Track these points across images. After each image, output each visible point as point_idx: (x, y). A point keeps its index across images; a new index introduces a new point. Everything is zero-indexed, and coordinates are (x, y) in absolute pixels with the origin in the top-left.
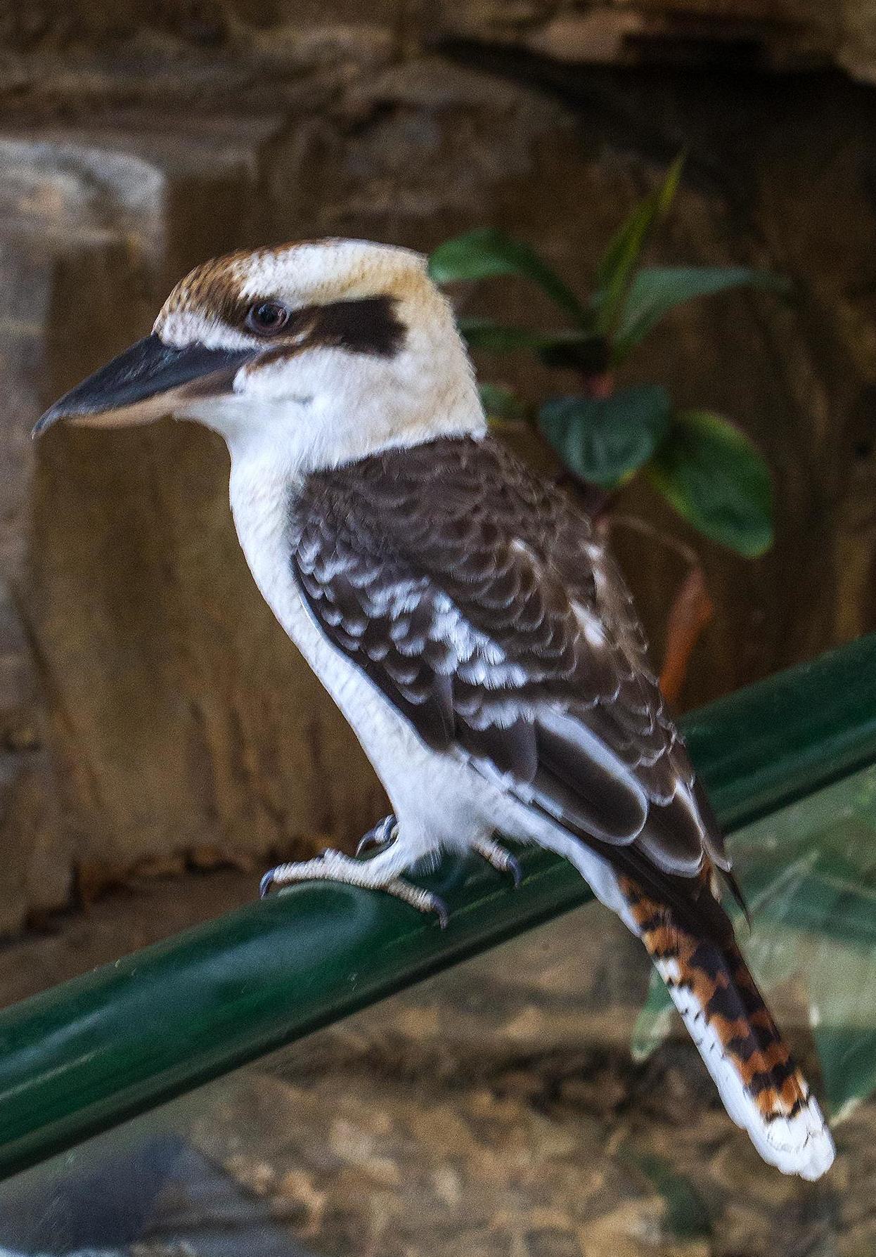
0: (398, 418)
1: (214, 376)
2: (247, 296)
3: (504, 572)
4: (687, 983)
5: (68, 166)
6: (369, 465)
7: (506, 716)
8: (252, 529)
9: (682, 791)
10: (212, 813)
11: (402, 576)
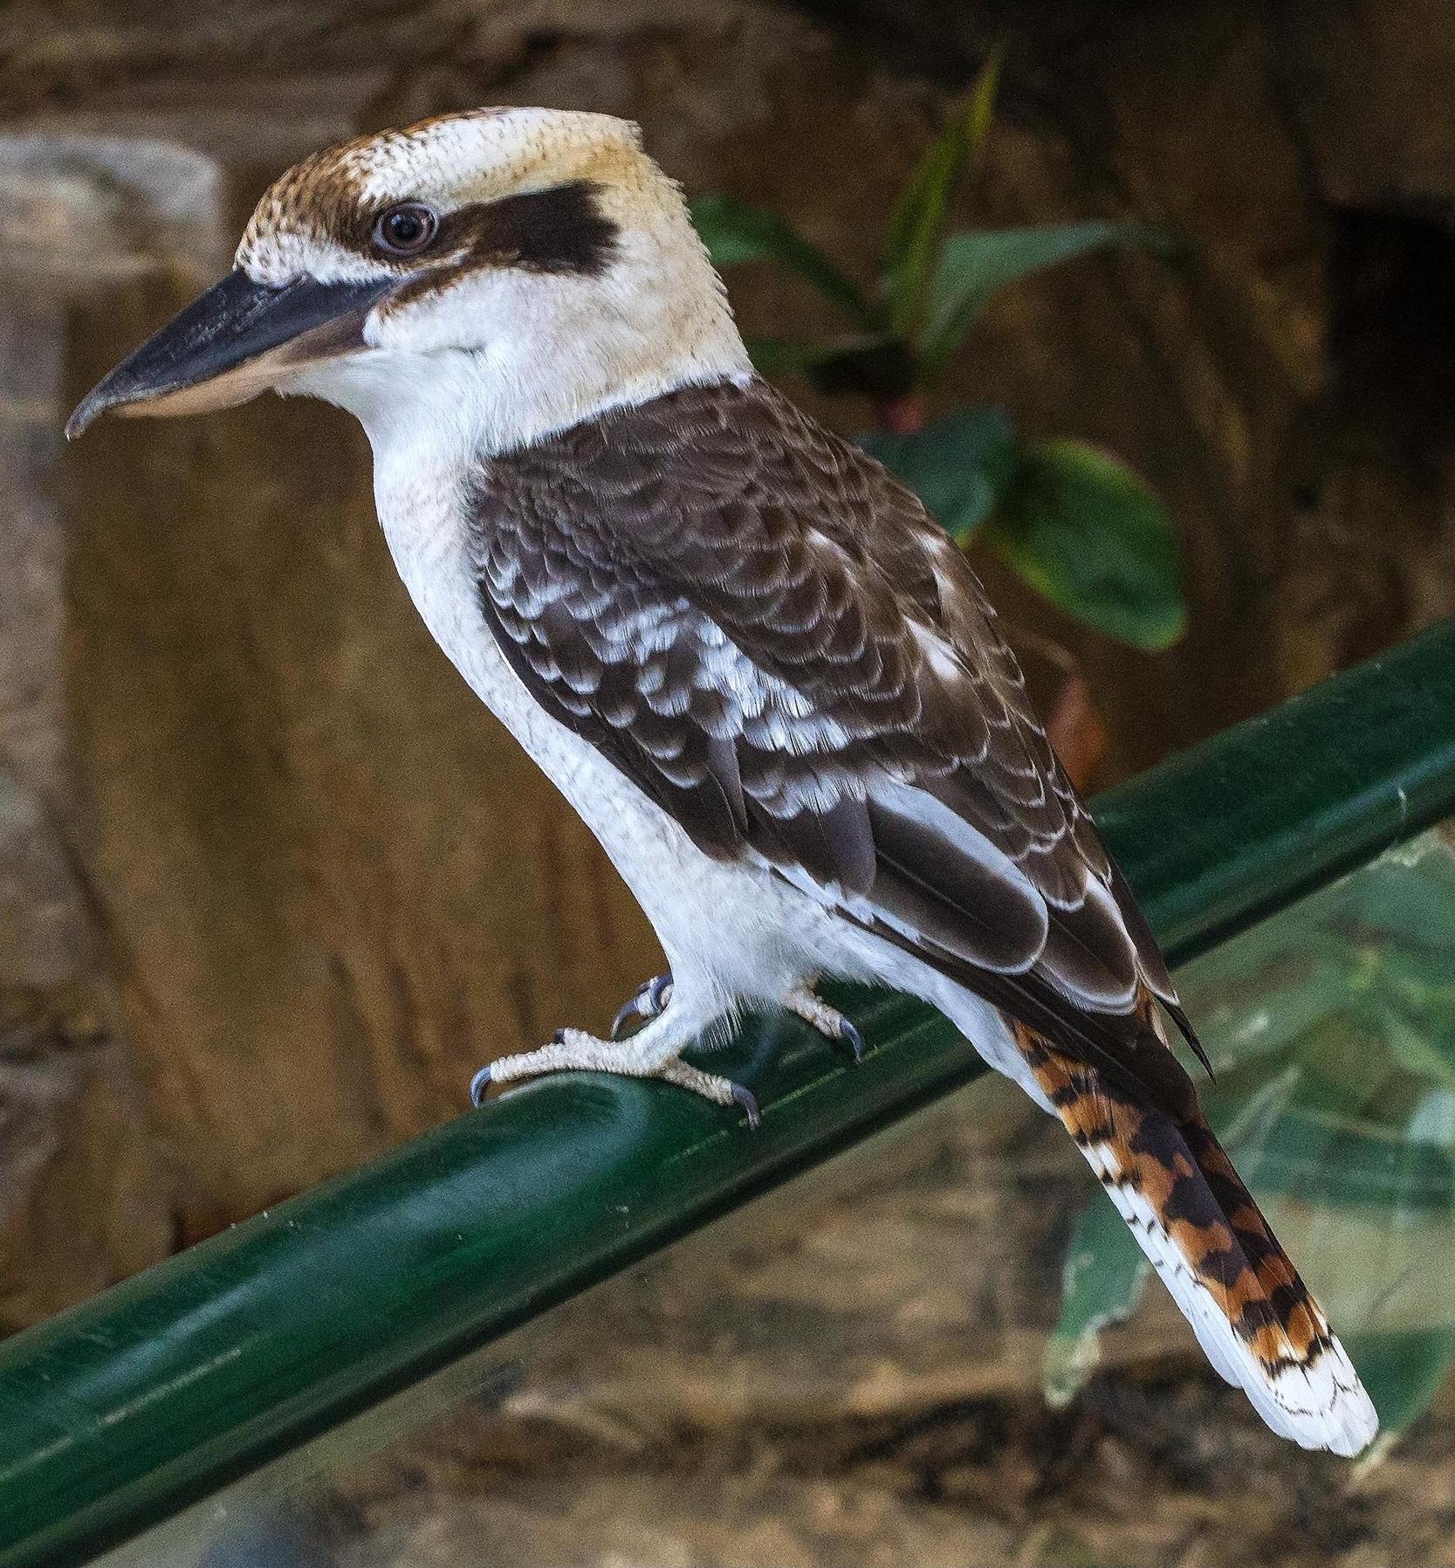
0: (616, 363)
1: (330, 326)
2: (373, 198)
3: (799, 580)
4: (1131, 1177)
5: (73, 166)
6: (581, 437)
7: (823, 795)
8: (413, 553)
9: (1096, 886)
10: (376, 1120)
11: (648, 597)
